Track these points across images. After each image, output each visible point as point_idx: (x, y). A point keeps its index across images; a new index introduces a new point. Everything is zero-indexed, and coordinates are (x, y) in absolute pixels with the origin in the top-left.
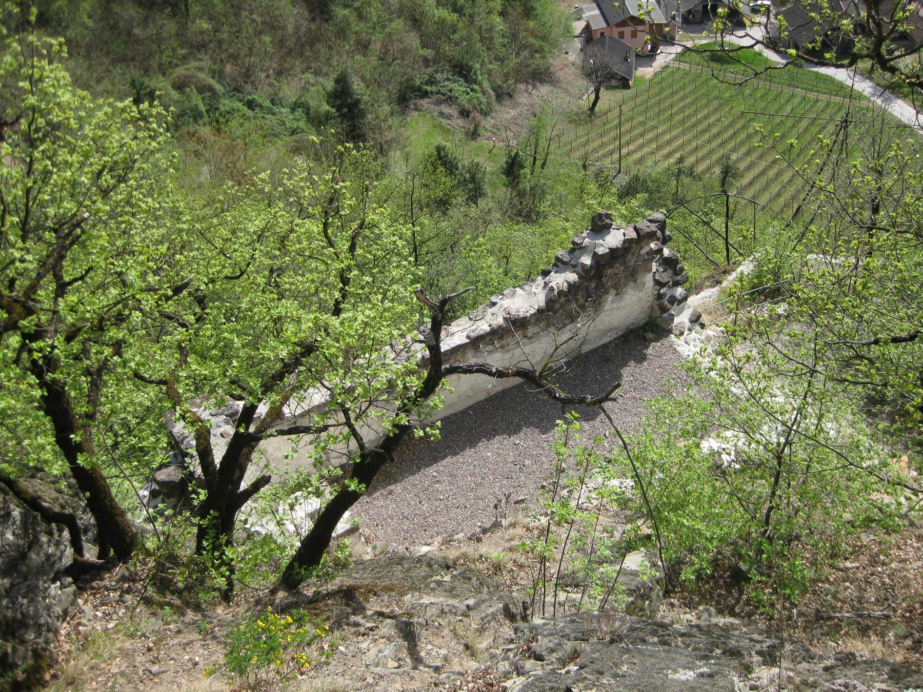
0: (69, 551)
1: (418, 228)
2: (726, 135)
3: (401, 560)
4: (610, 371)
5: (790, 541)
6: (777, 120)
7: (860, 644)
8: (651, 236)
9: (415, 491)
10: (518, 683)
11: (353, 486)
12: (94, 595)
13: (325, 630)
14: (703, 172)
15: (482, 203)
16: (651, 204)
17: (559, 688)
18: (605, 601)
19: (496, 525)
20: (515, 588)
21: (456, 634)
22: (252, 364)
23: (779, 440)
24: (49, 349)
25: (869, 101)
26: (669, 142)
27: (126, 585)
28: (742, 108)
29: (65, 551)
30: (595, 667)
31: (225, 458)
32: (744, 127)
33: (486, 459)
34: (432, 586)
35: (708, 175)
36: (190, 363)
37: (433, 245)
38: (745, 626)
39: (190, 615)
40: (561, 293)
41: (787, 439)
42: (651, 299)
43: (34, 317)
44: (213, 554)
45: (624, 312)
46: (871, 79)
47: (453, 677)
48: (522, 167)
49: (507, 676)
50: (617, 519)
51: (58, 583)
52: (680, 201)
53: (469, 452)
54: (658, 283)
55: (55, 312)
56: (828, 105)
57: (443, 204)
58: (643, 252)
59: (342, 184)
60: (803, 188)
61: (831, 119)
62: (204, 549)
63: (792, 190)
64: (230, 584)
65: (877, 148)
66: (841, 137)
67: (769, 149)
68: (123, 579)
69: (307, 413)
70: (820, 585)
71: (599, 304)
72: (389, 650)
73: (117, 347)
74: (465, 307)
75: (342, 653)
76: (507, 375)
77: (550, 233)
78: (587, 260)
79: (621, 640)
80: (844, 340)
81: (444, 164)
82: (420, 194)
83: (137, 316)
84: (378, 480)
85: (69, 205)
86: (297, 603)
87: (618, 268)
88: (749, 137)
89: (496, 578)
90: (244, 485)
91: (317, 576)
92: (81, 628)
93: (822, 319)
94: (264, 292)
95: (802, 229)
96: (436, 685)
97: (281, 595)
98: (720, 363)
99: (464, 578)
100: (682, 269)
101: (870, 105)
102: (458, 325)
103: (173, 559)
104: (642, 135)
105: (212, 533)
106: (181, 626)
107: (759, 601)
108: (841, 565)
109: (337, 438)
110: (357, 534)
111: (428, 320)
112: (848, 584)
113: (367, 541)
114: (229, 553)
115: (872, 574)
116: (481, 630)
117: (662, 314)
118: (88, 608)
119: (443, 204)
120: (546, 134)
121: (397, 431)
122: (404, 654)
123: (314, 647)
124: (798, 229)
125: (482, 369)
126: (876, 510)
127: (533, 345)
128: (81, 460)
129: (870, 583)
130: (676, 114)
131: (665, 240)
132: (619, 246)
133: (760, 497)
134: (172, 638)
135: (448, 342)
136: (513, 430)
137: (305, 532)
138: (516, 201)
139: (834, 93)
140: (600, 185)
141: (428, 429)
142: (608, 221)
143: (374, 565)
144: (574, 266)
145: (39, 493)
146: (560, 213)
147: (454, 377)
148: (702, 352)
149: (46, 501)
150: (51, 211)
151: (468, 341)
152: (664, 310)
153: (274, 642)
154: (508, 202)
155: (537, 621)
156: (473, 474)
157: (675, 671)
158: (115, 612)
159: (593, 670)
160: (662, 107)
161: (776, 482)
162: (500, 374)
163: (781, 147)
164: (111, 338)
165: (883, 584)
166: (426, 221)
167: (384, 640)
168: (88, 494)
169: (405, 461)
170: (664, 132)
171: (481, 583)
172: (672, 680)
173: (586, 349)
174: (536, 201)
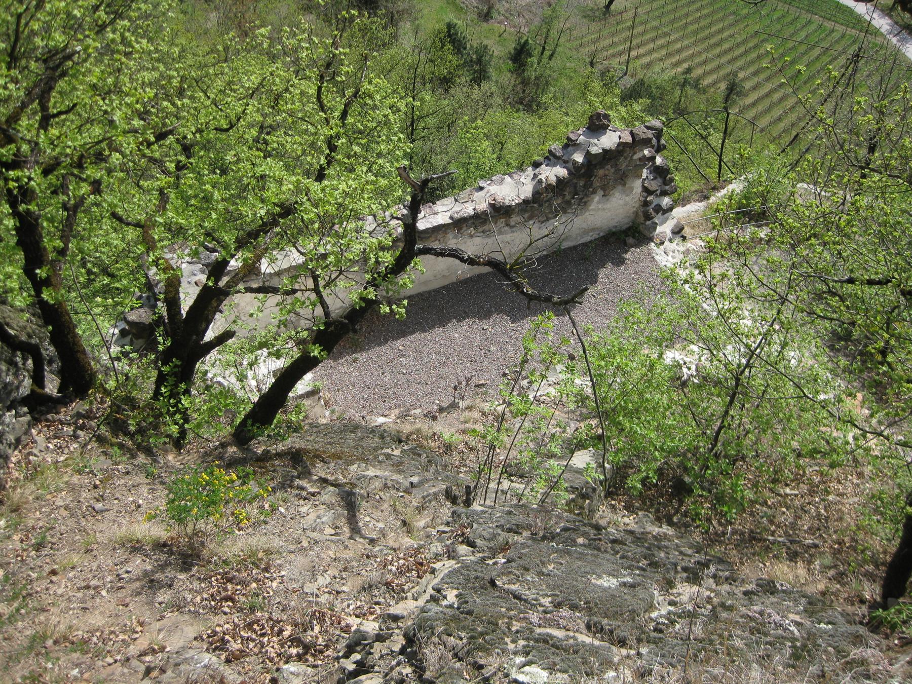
0: (27, 382)
1: (418, 103)
2: (737, 52)
3: (356, 428)
4: (586, 270)
5: (735, 461)
6: (790, 44)
7: (786, 568)
8: (646, 142)
9: (380, 362)
10: (447, 566)
11: (316, 352)
12: (48, 427)
13: (268, 490)
14: (708, 86)
15: (485, 85)
16: (651, 110)
17: (483, 578)
18: (546, 495)
19: (454, 406)
20: (463, 469)
21: (395, 510)
22: (230, 217)
23: (740, 360)
24: (26, 180)
25: (885, 38)
26: (679, 51)
27: (81, 421)
28: (757, 28)
29: (23, 381)
30: (522, 562)
31: (191, 308)
32: (756, 47)
33: (452, 340)
34: (380, 458)
35: (712, 90)
36: (168, 210)
37: (431, 121)
38: (677, 538)
39: (142, 459)
40: (549, 186)
41: (748, 361)
42: (637, 205)
43: (13, 146)
44: (169, 401)
45: (609, 214)
46: (891, 17)
47: (386, 552)
48: (530, 56)
49: (437, 558)
50: (572, 416)
51: (14, 412)
52: (681, 112)
53: (437, 331)
54: (646, 190)
55: (37, 144)
56: (843, 36)
57: (446, 82)
58: (636, 157)
59: (341, 50)
60: (804, 116)
61: (844, 51)
62: (162, 395)
63: (792, 117)
64: (183, 433)
65: (884, 87)
66: (850, 71)
67: (776, 73)
68: (79, 415)
69: (278, 274)
70: (758, 506)
71: (585, 203)
72: (327, 517)
73: (96, 185)
74: (454, 187)
75: (281, 513)
76: (478, 264)
77: (548, 125)
78: (579, 158)
79: (553, 538)
80: (820, 275)
81: (453, 42)
82: (425, 69)
83: (116, 158)
84: (344, 346)
85: (59, 38)
86: (245, 459)
87: (609, 170)
88: (759, 57)
89: (446, 458)
90: (209, 336)
91: (269, 436)
92: (31, 458)
93: (803, 250)
94: (250, 148)
95: (796, 157)
96: (368, 557)
97: (232, 450)
98: (698, 277)
99: (414, 454)
100: (672, 180)
101: (885, 43)
102: (443, 205)
103: (131, 402)
104: (653, 40)
105: (171, 380)
106: (129, 467)
107: (697, 514)
108: (782, 491)
109: (304, 303)
110: (317, 397)
111: (409, 198)
112: (784, 509)
113: (327, 404)
114: (185, 402)
115: (809, 503)
116: (421, 509)
117: (645, 221)
118: (40, 439)
119: (446, 82)
120: (558, 25)
121: (363, 305)
122: (342, 522)
123: (255, 505)
124: (793, 156)
125: (454, 254)
126: (823, 442)
127: (515, 234)
128: (46, 295)
129: (806, 512)
130: (691, 24)
131: (659, 149)
132: (613, 148)
133: (713, 415)
134: (119, 479)
135: (431, 220)
136: (485, 315)
137: (266, 388)
138: (519, 88)
139: (851, 25)
140: (604, 85)
141: (394, 307)
142: (605, 122)
143: (328, 429)
144: (566, 162)
145: (8, 320)
146: (561, 107)
147: (430, 258)
148: (682, 264)
149: (13, 328)
150: (38, 41)
151: (450, 221)
152: (648, 217)
153: (216, 496)
154: (511, 88)
155: (476, 507)
156: (438, 353)
157: (600, 577)
158: (67, 446)
159: (519, 566)
160: (677, 14)
161: (731, 402)
162: (471, 262)
163: (790, 72)
164: (88, 177)
165: (819, 514)
166: (427, 98)
167: (324, 507)
168: (50, 328)
169: (373, 331)
170: (676, 41)
171: (429, 461)
172: (595, 585)
173: (566, 245)
174: (539, 91)
